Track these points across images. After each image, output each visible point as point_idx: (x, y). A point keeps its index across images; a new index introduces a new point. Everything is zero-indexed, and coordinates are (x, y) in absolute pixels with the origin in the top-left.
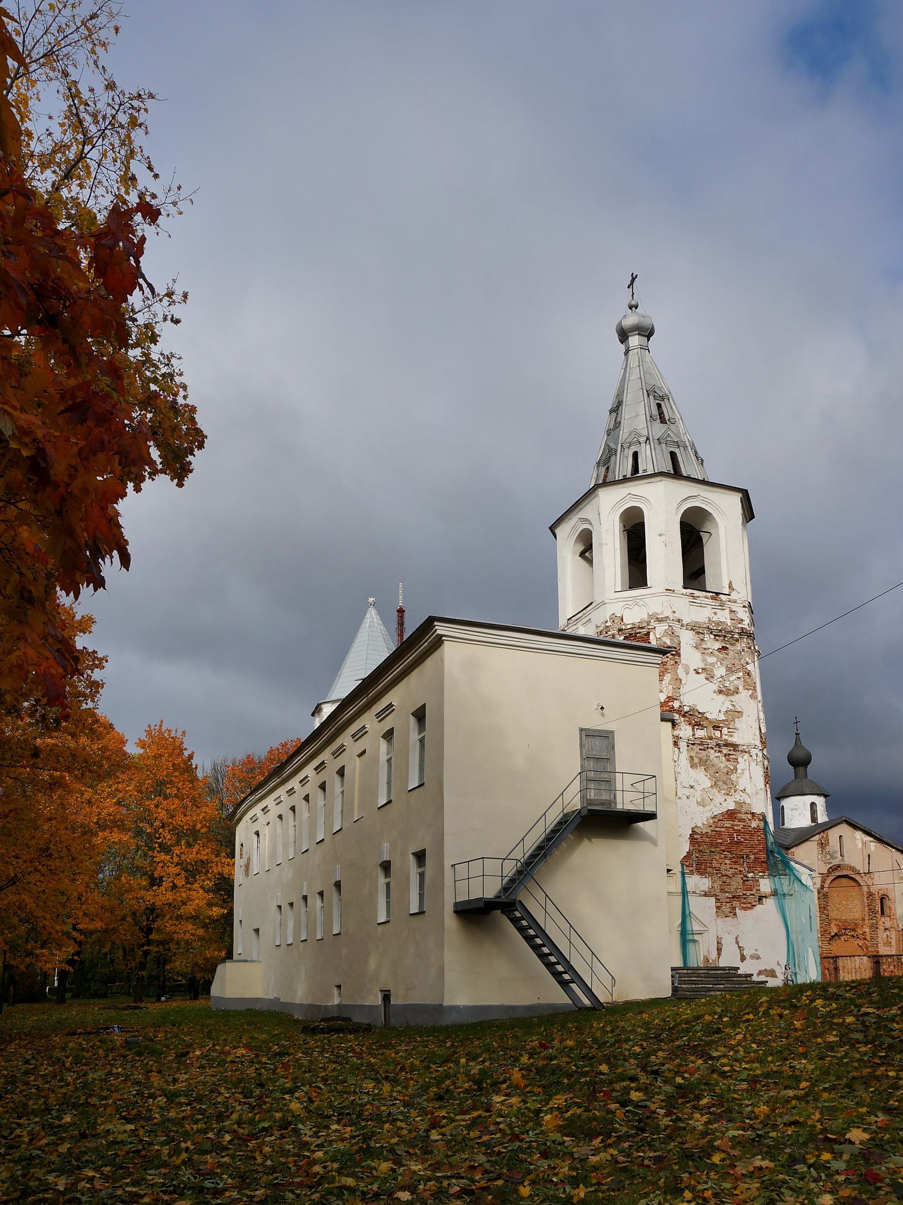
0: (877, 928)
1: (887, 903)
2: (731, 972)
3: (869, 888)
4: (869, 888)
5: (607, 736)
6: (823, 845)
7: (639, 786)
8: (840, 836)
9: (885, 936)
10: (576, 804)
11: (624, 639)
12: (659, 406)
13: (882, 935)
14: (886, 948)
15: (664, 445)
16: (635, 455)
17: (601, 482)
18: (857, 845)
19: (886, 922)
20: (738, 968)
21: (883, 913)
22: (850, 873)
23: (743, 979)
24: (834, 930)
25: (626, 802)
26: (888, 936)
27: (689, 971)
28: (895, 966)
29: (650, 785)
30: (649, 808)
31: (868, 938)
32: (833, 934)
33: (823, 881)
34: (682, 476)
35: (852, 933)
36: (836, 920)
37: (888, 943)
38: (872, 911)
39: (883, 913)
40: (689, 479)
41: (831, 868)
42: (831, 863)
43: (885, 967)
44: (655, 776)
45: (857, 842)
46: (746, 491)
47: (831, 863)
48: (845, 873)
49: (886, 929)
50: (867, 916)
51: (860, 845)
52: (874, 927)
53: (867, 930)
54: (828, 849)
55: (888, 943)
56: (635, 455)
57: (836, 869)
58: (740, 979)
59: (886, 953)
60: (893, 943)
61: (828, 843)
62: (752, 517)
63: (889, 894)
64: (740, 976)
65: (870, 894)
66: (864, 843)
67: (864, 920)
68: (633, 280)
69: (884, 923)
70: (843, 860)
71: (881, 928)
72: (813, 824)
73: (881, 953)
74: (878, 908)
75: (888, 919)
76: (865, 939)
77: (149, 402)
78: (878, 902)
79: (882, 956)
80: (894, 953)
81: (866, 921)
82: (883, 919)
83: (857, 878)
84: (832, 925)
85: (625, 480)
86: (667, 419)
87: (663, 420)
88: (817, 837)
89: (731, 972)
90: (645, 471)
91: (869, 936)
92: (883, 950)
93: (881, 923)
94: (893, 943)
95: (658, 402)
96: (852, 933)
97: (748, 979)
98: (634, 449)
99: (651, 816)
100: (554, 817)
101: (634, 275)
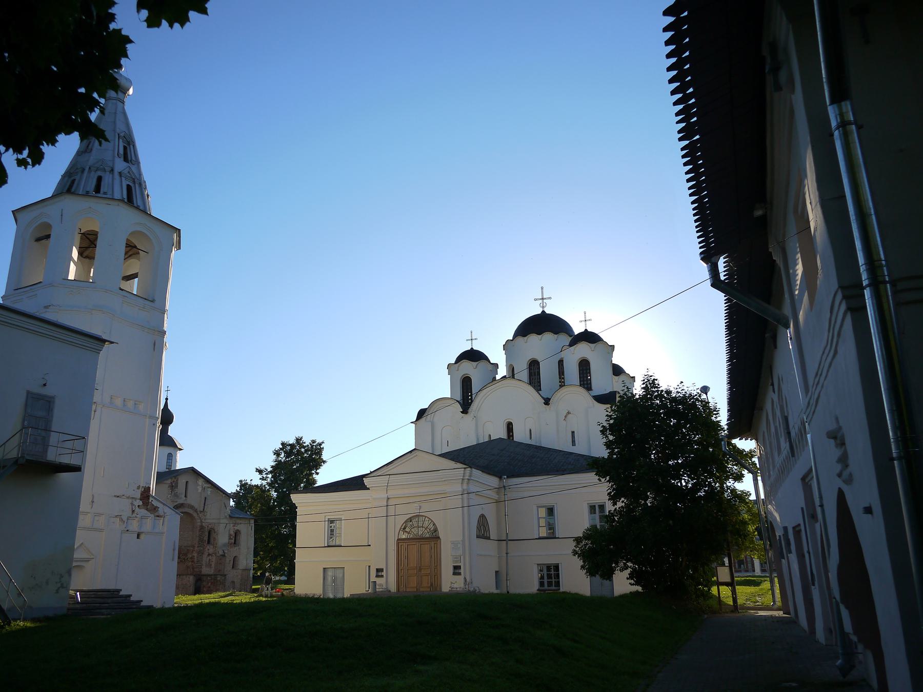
0: (203, 553)
5: (48, 403)
8: (187, 482)
9: (208, 560)
10: (14, 454)
11: (784, 559)
12: (125, 148)
13: (205, 559)
16: (100, 179)
18: (198, 489)
19: (210, 549)
21: (209, 542)
22: (191, 511)
25: (52, 456)
26: (210, 560)
28: (212, 583)
29: (78, 444)
31: (196, 560)
37: (209, 565)
39: (209, 542)
40: (137, 208)
42: (177, 502)
43: (205, 583)
45: (198, 487)
47: (177, 502)
49: (209, 555)
50: (197, 544)
51: (200, 489)
52: (201, 553)
53: (195, 555)
55: (209, 565)
56: (100, 179)
59: (207, 573)
60: (213, 565)
61: (177, 486)
64: (122, 596)
65: (202, 527)
66: (204, 489)
67: (194, 547)
72: (168, 470)
73: (203, 573)
74: (206, 538)
76: (192, 561)
77: (671, 413)
79: (204, 575)
81: (196, 548)
83: (195, 515)
85: (87, 194)
86: (129, 159)
87: (126, 159)
88: (169, 481)
90: (105, 193)
92: (205, 570)
93: (206, 549)
94: (213, 565)
97: (128, 598)
98: (99, 173)
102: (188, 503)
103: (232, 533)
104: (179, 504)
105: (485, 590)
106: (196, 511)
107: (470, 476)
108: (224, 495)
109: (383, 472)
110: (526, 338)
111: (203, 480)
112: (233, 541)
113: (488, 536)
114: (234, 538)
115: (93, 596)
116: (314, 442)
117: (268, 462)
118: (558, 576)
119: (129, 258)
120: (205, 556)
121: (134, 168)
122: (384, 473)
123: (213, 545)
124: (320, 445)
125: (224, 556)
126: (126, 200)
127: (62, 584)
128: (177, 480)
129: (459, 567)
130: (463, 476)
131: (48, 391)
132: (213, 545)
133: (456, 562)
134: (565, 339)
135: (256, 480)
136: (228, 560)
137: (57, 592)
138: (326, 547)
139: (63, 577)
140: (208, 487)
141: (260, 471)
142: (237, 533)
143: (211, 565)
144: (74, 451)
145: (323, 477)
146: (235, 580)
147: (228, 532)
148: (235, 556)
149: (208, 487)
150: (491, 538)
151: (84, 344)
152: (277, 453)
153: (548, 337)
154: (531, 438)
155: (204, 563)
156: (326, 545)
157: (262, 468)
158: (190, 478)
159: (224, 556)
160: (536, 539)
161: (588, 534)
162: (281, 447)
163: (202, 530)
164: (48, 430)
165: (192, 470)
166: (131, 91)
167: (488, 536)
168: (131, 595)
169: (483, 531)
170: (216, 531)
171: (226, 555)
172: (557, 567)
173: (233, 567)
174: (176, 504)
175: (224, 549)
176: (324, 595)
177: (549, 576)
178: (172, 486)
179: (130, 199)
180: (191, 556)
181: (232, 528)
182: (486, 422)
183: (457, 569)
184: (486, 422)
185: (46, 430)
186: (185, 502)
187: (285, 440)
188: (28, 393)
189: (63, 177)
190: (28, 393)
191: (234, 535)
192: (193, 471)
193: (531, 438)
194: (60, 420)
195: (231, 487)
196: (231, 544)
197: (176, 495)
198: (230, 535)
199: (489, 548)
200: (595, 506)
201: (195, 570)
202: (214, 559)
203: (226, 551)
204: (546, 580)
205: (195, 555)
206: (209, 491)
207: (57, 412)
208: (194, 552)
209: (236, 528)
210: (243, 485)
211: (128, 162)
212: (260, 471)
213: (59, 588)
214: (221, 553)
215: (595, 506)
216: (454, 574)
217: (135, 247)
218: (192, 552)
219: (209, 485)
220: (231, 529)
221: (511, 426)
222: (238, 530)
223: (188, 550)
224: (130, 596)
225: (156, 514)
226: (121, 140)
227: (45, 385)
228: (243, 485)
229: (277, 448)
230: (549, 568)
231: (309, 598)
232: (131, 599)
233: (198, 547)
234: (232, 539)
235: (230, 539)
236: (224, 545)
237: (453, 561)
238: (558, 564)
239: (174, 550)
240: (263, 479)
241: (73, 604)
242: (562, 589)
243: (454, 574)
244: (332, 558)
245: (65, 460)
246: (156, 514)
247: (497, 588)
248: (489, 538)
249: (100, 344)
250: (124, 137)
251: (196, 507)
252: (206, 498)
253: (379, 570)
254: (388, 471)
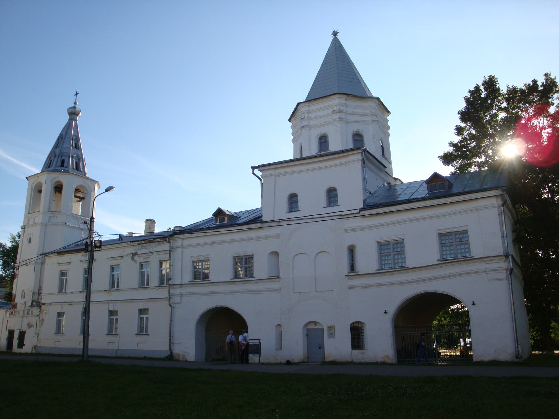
68: (77, 94)
98: (63, 158)
101: (77, 92)
121: (79, 153)
166: (80, 114)
179: (78, 168)
189: (47, 158)
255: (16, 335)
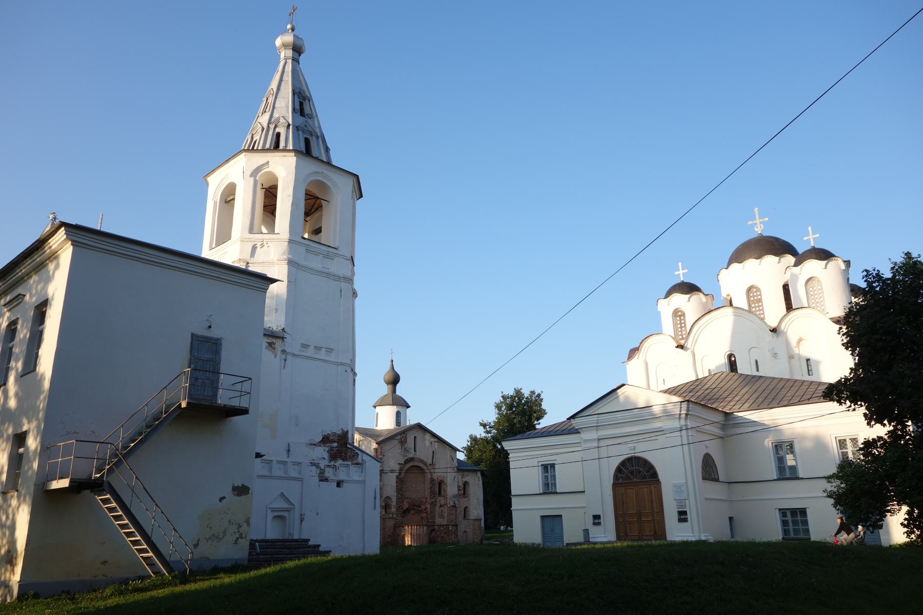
1: (443, 486)
2: (286, 544)
3: (432, 475)
4: (432, 475)
5: (215, 345)
6: (403, 442)
7: (238, 387)
8: (415, 437)
14: (441, 520)
15: (301, 133)
17: (246, 148)
18: (426, 444)
20: (319, 545)
22: (421, 465)
23: (312, 549)
24: (406, 506)
25: (224, 398)
26: (442, 511)
27: (269, 544)
29: (246, 386)
30: (243, 403)
31: (429, 512)
32: (405, 509)
33: (401, 469)
34: (312, 156)
35: (418, 508)
36: (408, 498)
37: (441, 516)
38: (432, 492)
40: (317, 159)
41: (407, 460)
43: (155, 592)
44: (250, 379)
46: (357, 177)
47: (407, 456)
48: (416, 464)
49: (441, 506)
50: (429, 496)
51: (428, 444)
52: (433, 504)
53: (428, 506)
54: (406, 445)
55: (441, 516)
57: (411, 461)
58: (309, 549)
60: (446, 516)
61: (406, 442)
62: (361, 196)
63: (445, 480)
64: (310, 547)
65: (432, 480)
69: (440, 501)
70: (415, 454)
71: (438, 505)
75: (443, 498)
76: (427, 513)
78: (437, 486)
80: (445, 523)
81: (428, 500)
82: (439, 498)
83: (425, 468)
84: (405, 502)
85: (269, 150)
88: (399, 437)
89: (303, 543)
91: (429, 510)
93: (438, 500)
94: (446, 516)
95: (300, 100)
96: (418, 508)
97: (316, 549)
99: (244, 411)
100: (154, 408)
102: (418, 457)
103: (461, 484)
104: (409, 458)
105: (725, 539)
106: (426, 465)
107: (688, 410)
108: (450, 448)
109: (591, 412)
110: (742, 264)
111: (430, 435)
112: (462, 492)
113: (716, 477)
114: (463, 490)
115: (278, 547)
116: (533, 392)
117: (492, 416)
118: (805, 523)
119: (316, 212)
120: (437, 508)
122: (592, 413)
123: (444, 496)
124: (539, 395)
125: (454, 506)
126: (305, 152)
127: (241, 535)
128: (406, 436)
129: (685, 513)
130: (681, 411)
131: (215, 333)
132: (444, 496)
133: (682, 506)
134: (790, 259)
135: (480, 433)
136: (459, 511)
137: (236, 543)
138: (540, 494)
139: (241, 527)
140: (435, 442)
141: (484, 425)
142: (466, 484)
143: (443, 516)
144: (243, 393)
145: (543, 423)
146: (468, 530)
147: (457, 483)
148: (466, 507)
149: (435, 442)
150: (720, 480)
151: (255, 285)
152: (498, 407)
153: (770, 260)
154: (758, 371)
155: (437, 513)
156: (541, 492)
157: (485, 422)
158: (419, 434)
159: (454, 506)
160: (775, 480)
161: (842, 465)
162: (502, 400)
163: (433, 482)
164: (217, 372)
165: (419, 425)
167: (716, 477)
168: (319, 545)
169: (709, 470)
170: (446, 482)
171: (457, 506)
172: (803, 512)
173: (464, 518)
174: (406, 458)
175: (454, 499)
176: (543, 545)
177: (795, 523)
178: (402, 442)
180: (424, 507)
181: (460, 479)
182: (703, 357)
183: (682, 516)
184: (703, 357)
185: (213, 372)
186: (415, 457)
187: (506, 393)
188: (193, 335)
190: (193, 335)
191: (463, 486)
192: (419, 427)
193: (758, 371)
194: (229, 362)
195: (460, 441)
196: (460, 495)
197: (406, 450)
198: (459, 487)
199: (714, 490)
200: (845, 440)
201: (429, 520)
202: (445, 509)
203: (457, 502)
204: (791, 527)
205: (428, 506)
206: (436, 445)
207: (224, 354)
208: (427, 503)
209: (465, 480)
210: (474, 439)
211: (304, 116)
212: (484, 425)
213: (237, 539)
214: (452, 503)
215: (845, 440)
216: (680, 520)
217: (318, 198)
218: (425, 503)
219: (436, 440)
220: (460, 480)
221: (733, 359)
222: (466, 481)
223: (421, 501)
224: (319, 546)
225: (355, 461)
226: (296, 96)
227: (210, 327)
228: (474, 439)
229: (498, 401)
230: (794, 512)
231: (755, 542)
232: (320, 550)
233: (430, 498)
234: (461, 490)
235: (459, 490)
236: (455, 496)
237: (677, 505)
238: (805, 508)
239: (375, 498)
240: (488, 432)
241: (255, 555)
242: (813, 538)
243: (680, 520)
244: (550, 505)
245: (235, 403)
246: (355, 461)
247: (732, 536)
248: (717, 480)
249: (265, 282)
250: (299, 93)
251: (425, 461)
252: (433, 452)
253: (597, 517)
254: (598, 409)
255: (327, 350)
